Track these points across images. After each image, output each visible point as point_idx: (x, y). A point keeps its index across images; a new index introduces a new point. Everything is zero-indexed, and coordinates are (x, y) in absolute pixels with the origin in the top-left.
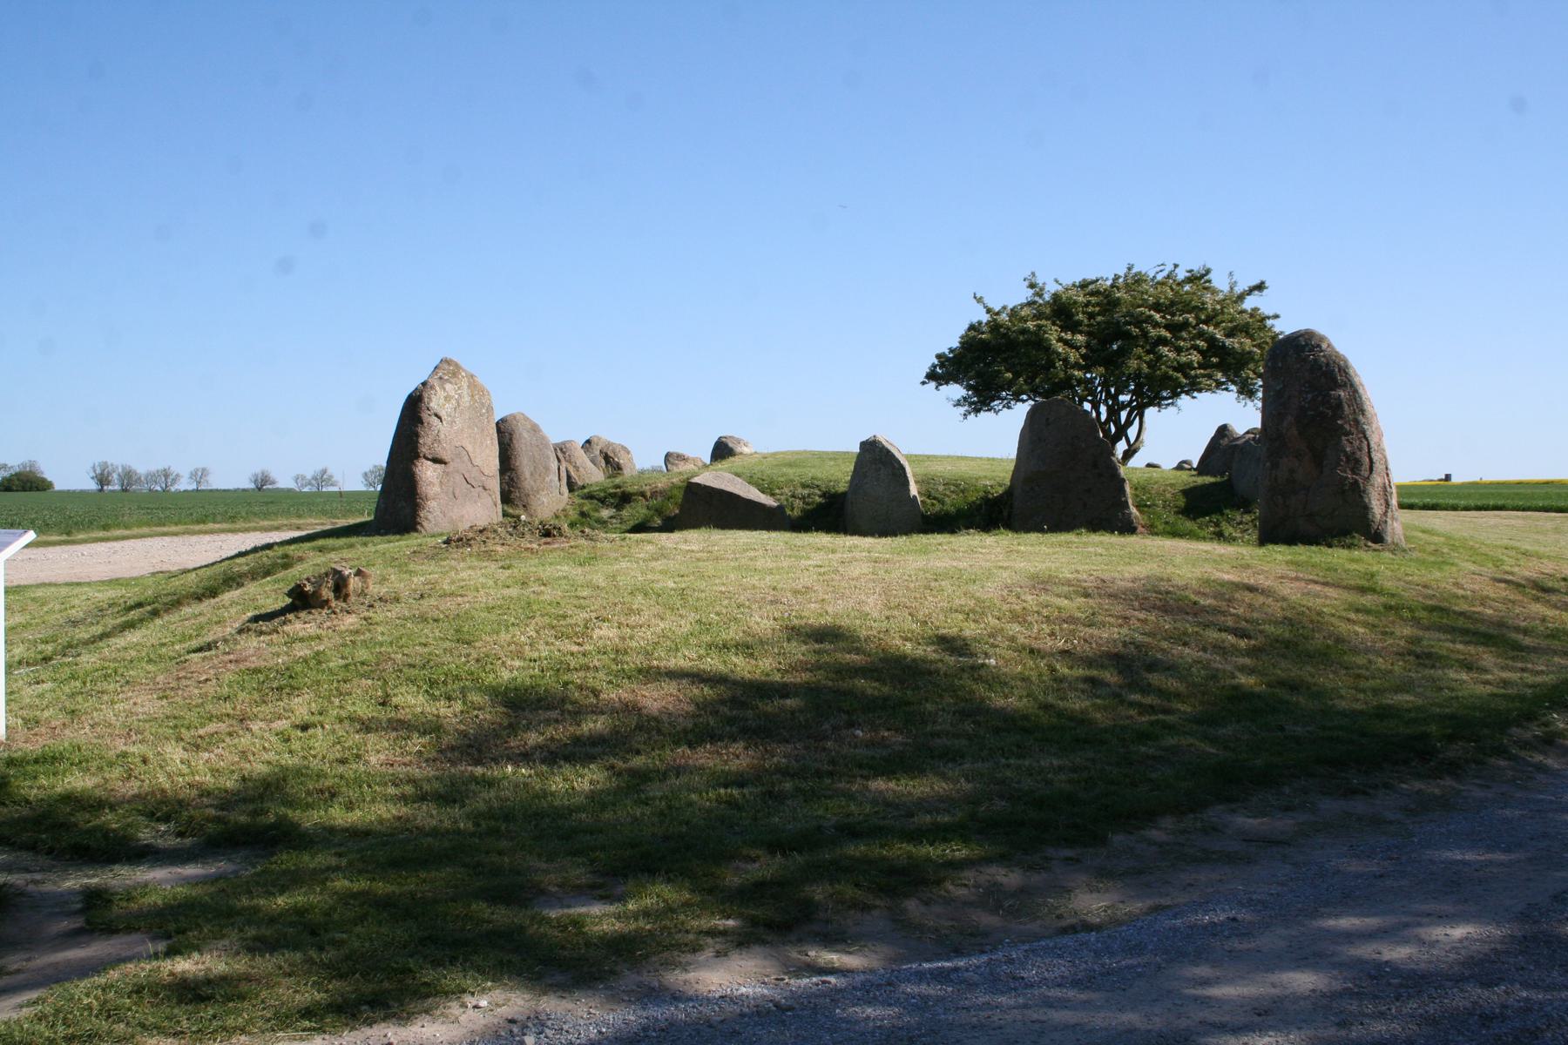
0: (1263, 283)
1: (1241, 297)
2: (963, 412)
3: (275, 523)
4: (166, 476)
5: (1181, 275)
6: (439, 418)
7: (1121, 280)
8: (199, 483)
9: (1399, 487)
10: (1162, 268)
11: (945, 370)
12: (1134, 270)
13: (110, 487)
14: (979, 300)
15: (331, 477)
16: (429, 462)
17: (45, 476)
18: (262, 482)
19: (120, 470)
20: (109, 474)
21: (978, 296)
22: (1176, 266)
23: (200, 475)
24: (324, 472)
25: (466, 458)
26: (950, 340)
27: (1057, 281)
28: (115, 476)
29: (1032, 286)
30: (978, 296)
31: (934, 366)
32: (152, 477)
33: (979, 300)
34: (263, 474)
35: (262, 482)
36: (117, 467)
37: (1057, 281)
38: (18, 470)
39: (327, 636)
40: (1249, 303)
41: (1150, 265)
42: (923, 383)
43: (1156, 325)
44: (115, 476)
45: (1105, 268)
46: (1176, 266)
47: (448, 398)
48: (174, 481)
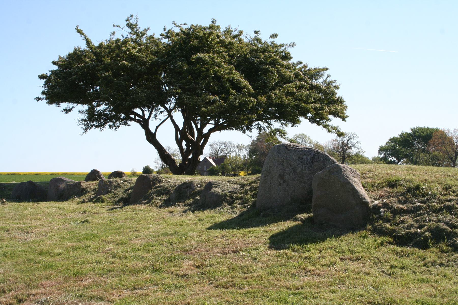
2: (84, 127)
14: (79, 31)
33: (79, 31)
42: (38, 99)
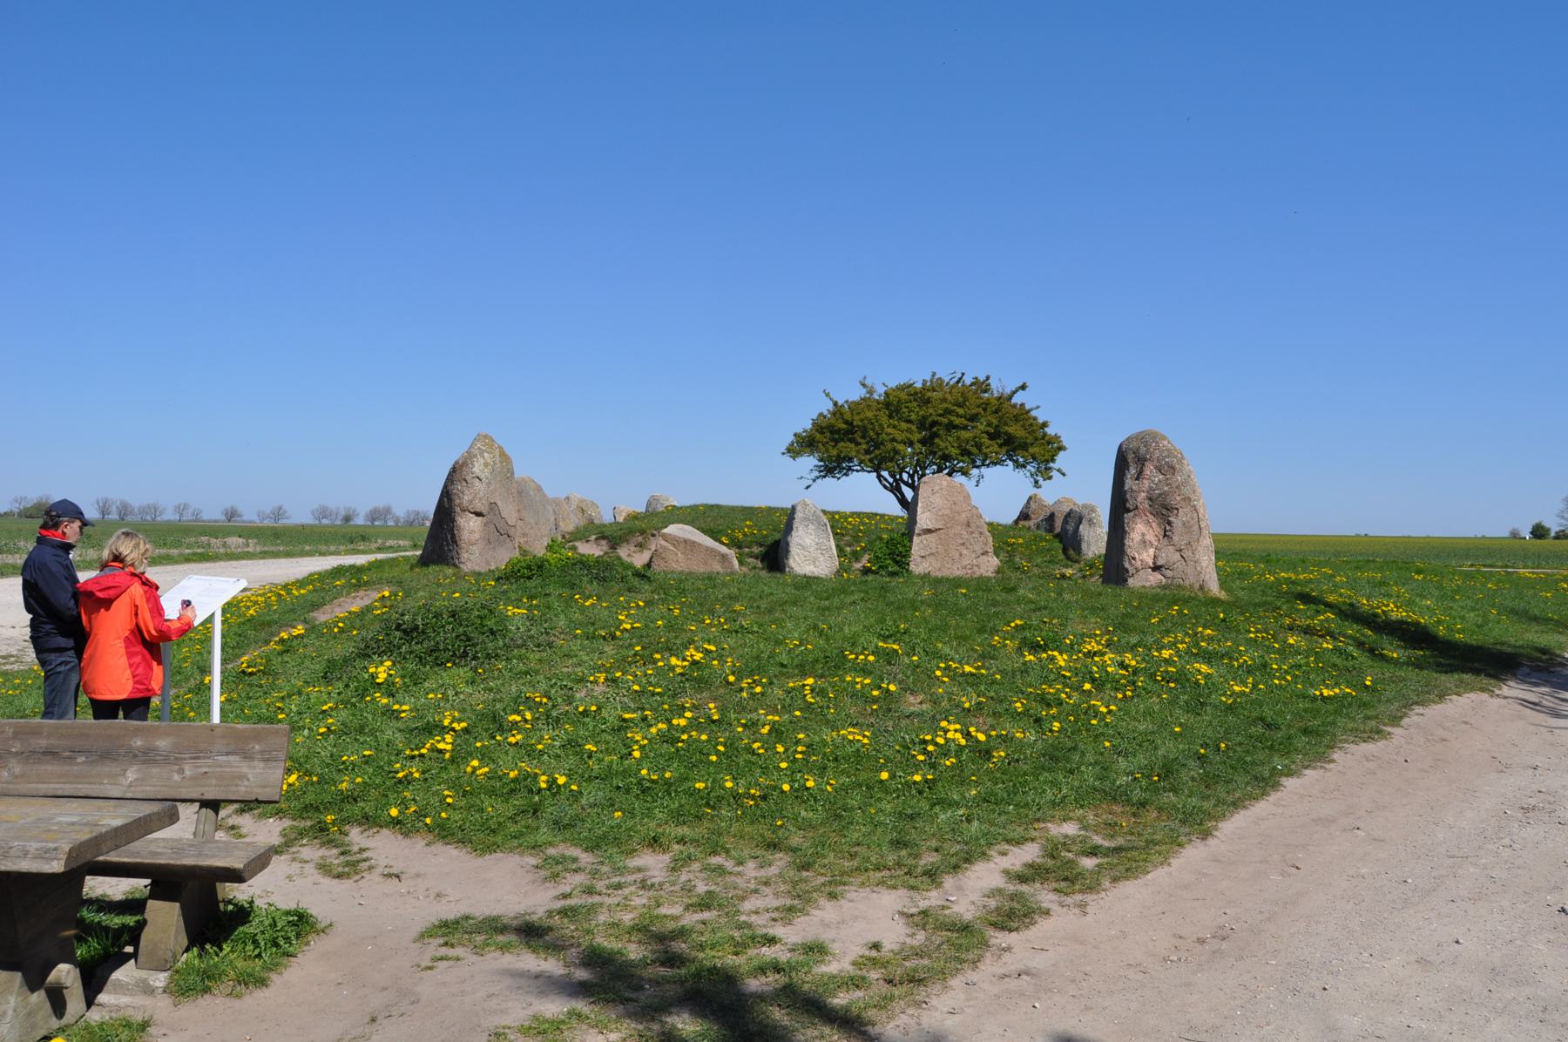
0: (1025, 383)
1: (1010, 398)
3: (273, 548)
4: (156, 509)
5: (968, 380)
6: (480, 480)
7: (929, 384)
8: (181, 515)
9: (1217, 538)
10: (952, 376)
11: (804, 444)
12: (936, 377)
13: (110, 517)
15: (285, 512)
16: (471, 515)
17: (51, 502)
18: (231, 514)
19: (118, 504)
20: (110, 506)
21: (827, 392)
22: (963, 374)
23: (181, 509)
24: (280, 508)
25: (497, 512)
26: (805, 424)
27: (884, 384)
28: (114, 508)
29: (864, 385)
30: (827, 392)
31: (792, 444)
32: (144, 510)
34: (232, 508)
35: (231, 514)
36: (116, 501)
37: (884, 384)
38: (35, 501)
39: (1013, 792)
40: (1017, 400)
41: (945, 375)
42: (783, 454)
43: (958, 416)
44: (114, 508)
45: (918, 376)
46: (963, 374)
47: (486, 465)
48: (161, 513)
